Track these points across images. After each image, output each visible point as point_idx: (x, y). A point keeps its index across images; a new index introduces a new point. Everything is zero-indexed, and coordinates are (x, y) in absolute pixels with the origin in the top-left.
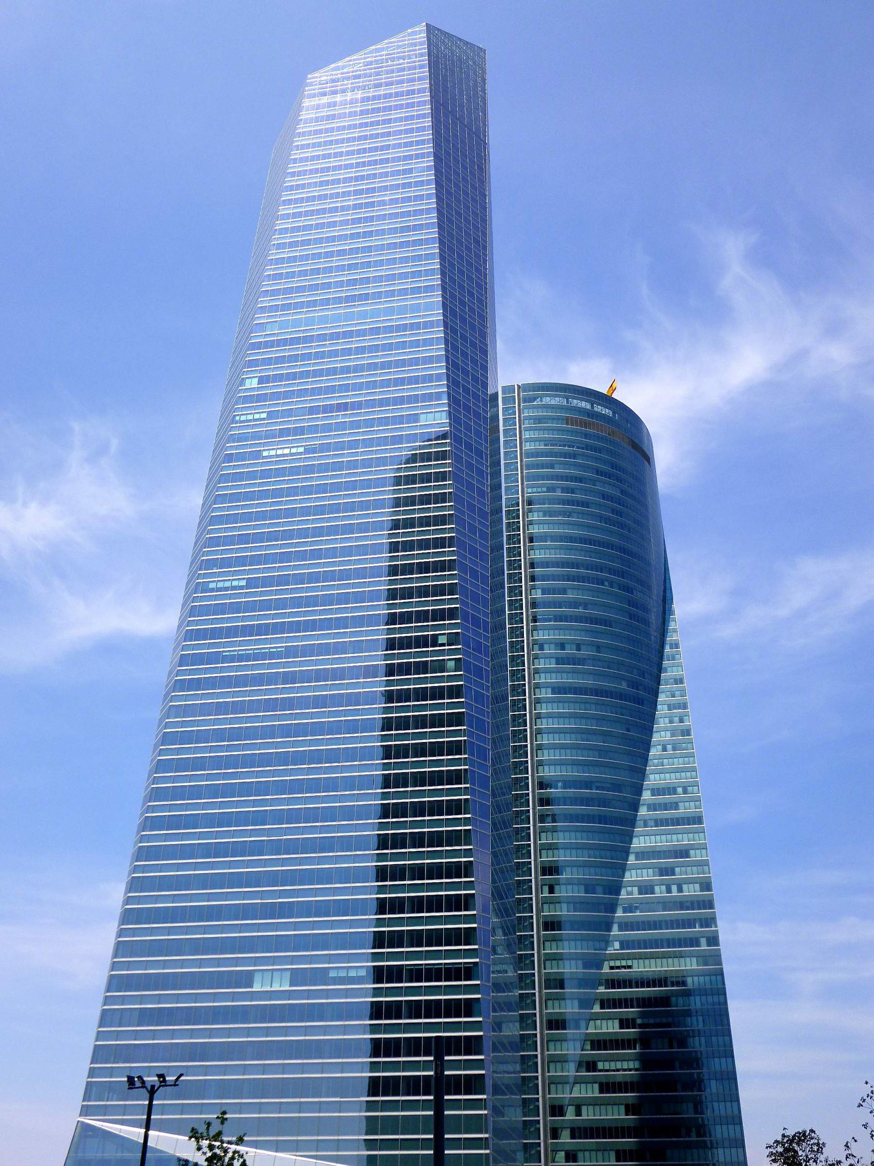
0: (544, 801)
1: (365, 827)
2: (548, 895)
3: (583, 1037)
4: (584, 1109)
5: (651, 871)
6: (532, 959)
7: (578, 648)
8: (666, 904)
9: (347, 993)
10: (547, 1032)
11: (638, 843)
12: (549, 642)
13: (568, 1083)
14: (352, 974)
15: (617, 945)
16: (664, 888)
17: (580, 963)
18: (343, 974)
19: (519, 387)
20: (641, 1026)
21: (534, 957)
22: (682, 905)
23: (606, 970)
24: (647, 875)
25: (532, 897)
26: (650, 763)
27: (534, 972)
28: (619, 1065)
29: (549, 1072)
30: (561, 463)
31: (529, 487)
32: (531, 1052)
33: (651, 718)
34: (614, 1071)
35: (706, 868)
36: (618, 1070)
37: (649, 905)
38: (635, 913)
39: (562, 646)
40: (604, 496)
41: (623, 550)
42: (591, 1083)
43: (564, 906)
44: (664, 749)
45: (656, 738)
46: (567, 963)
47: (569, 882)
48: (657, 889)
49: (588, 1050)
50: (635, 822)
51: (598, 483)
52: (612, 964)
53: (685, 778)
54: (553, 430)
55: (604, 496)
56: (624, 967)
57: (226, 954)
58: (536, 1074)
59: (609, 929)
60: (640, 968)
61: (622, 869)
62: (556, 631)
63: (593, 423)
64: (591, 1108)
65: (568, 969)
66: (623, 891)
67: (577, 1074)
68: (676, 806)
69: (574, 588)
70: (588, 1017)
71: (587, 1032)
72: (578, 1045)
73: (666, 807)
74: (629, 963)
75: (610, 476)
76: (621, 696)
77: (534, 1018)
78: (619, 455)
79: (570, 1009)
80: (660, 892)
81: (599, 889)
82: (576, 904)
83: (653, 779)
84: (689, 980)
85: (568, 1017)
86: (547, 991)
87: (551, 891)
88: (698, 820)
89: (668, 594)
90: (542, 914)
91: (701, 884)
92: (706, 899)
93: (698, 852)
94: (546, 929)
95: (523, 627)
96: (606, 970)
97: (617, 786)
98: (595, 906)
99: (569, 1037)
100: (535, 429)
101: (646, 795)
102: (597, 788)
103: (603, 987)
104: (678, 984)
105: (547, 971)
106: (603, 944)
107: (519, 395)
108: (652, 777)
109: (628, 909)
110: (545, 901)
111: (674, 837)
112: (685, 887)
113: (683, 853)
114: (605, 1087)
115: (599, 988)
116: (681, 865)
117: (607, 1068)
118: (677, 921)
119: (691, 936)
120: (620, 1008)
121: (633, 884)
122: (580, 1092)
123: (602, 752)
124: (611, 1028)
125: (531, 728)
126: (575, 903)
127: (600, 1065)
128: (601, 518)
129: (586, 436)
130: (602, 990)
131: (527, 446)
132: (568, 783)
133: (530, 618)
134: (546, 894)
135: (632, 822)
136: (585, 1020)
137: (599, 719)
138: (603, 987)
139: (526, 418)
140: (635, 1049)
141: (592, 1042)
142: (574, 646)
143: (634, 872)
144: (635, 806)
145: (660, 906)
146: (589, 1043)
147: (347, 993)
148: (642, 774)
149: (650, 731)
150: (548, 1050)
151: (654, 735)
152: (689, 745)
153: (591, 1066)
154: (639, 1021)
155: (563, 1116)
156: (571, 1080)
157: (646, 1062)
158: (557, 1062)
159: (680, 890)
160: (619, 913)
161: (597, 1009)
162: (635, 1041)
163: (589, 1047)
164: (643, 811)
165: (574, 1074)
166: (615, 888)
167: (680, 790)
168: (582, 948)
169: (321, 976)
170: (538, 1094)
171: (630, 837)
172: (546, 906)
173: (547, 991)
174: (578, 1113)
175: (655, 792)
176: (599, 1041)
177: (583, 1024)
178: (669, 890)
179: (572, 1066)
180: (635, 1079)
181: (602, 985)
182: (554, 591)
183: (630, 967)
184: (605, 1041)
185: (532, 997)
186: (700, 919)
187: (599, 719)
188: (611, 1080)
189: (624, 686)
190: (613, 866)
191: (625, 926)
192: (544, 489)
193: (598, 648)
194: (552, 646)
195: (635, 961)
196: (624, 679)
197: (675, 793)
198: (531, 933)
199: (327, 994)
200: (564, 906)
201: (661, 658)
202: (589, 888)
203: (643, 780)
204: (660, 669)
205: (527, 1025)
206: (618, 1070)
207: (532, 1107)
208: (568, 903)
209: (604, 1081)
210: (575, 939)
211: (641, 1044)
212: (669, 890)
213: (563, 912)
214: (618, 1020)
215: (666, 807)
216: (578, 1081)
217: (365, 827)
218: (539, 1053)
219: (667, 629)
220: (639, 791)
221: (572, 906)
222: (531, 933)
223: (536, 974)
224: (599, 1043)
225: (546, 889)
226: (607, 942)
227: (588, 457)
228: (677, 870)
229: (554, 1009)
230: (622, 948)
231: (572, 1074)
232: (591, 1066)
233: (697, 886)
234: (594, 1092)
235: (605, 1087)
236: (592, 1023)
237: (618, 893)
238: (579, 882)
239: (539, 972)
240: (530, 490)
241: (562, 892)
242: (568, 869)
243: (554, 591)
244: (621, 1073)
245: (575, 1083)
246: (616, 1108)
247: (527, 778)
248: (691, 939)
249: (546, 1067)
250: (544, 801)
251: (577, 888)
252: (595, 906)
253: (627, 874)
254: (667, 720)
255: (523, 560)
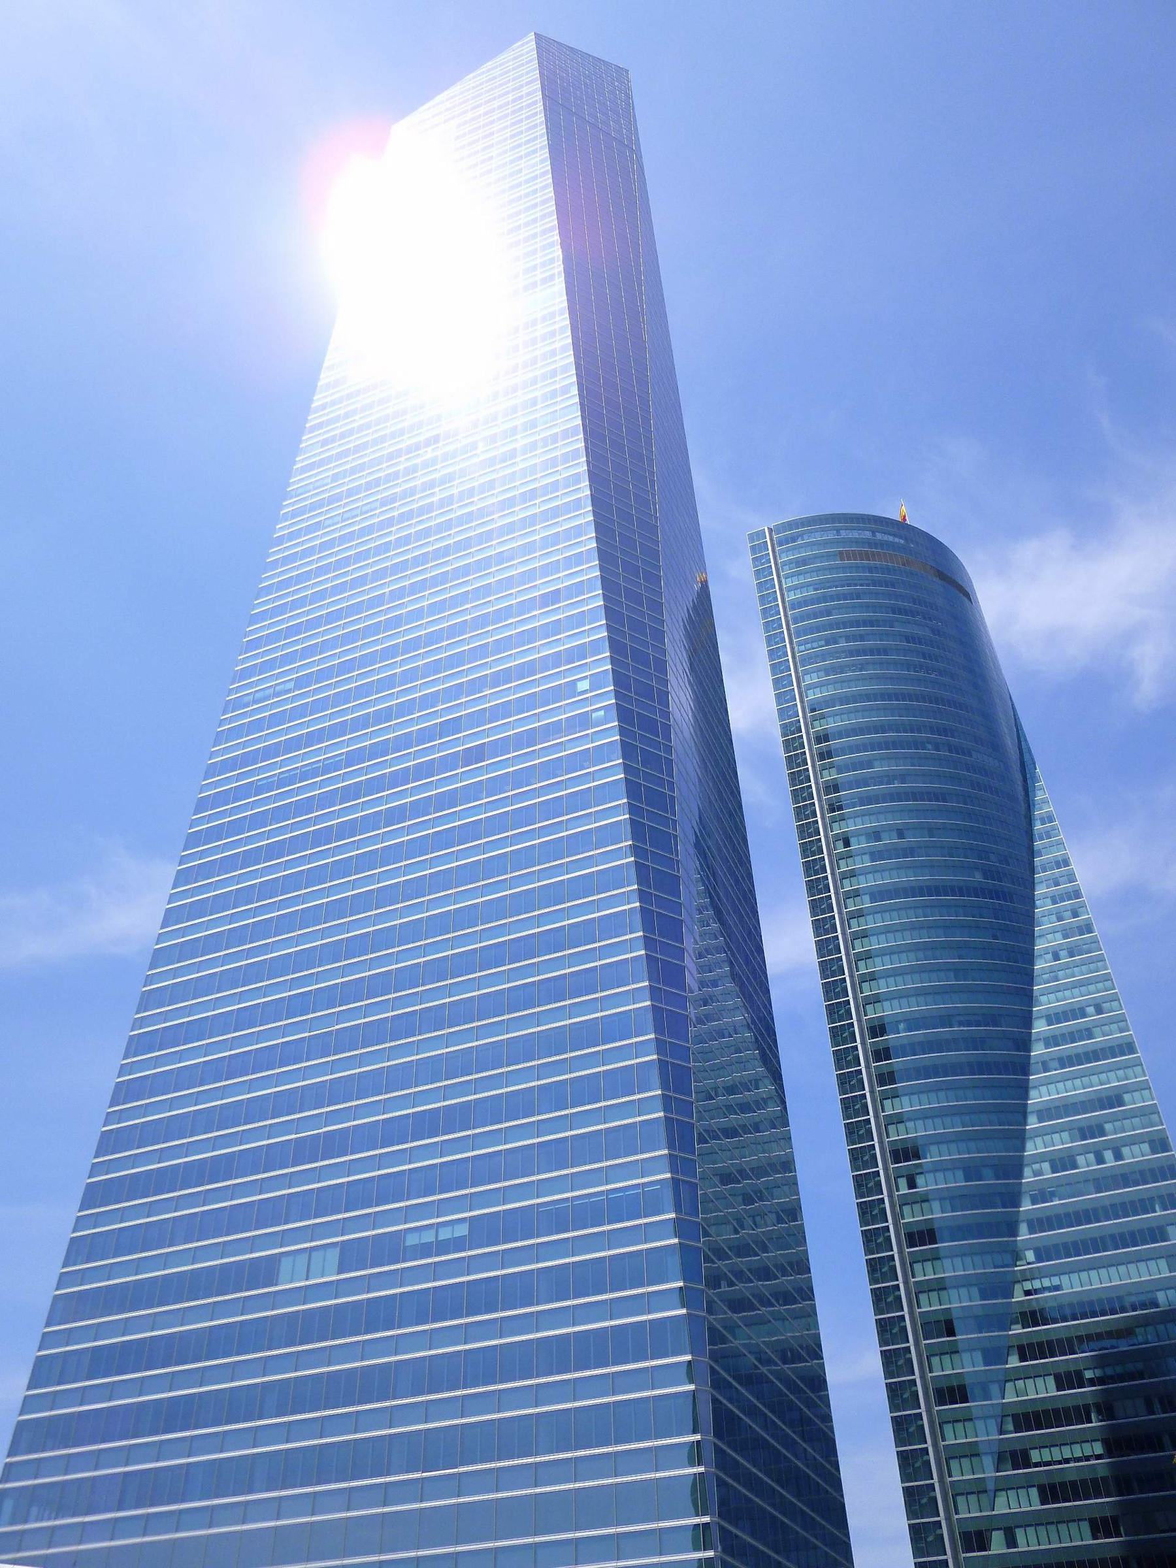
0: (882, 1054)
1: (657, 1458)
2: (907, 1192)
3: (998, 1411)
4: (1020, 1534)
5: (1065, 1135)
6: (920, 1423)
7: (901, 835)
8: (1099, 1182)
9: (436, 1271)
10: (908, 1250)
11: (1038, 1098)
12: (857, 833)
13: (986, 1491)
14: (445, 1234)
15: (1030, 1255)
16: (1091, 1157)
17: (975, 1291)
18: (428, 1237)
19: (770, 530)
20: (1092, 1382)
21: (874, 1149)
22: (1124, 1179)
23: (1019, 1297)
24: (1061, 1143)
25: (874, 1145)
26: (1036, 980)
27: (873, 1143)
28: (1067, 1452)
29: (898, 1190)
30: (840, 607)
31: (800, 644)
32: (894, 1312)
33: (1030, 919)
34: (1060, 1463)
35: (1155, 1117)
36: (1067, 1461)
37: (1073, 1186)
38: (1052, 1201)
39: (876, 835)
40: (908, 638)
41: (997, 894)
42: (1024, 1487)
43: (936, 1205)
44: (1056, 957)
45: (1040, 946)
46: (953, 1293)
47: (938, 1168)
48: (1080, 1160)
49: (1011, 1432)
50: (1029, 1066)
51: (896, 624)
52: (1028, 1286)
53: (1096, 994)
54: (824, 569)
55: (908, 638)
56: (1049, 1289)
57: (445, 1319)
58: (913, 1377)
59: (1014, 1232)
60: (1073, 1286)
61: (1020, 1138)
62: (898, 978)
63: (879, 554)
64: (1031, 1530)
65: (958, 1302)
66: (1027, 1171)
67: (998, 1474)
68: (1088, 1033)
69: (882, 758)
70: (1001, 1377)
71: (1004, 1401)
72: (993, 1425)
73: (1072, 1037)
74: (1056, 1281)
75: (912, 613)
76: (977, 891)
77: (938, 1532)
78: (922, 577)
79: (969, 1366)
80: (1086, 1165)
81: (987, 1172)
82: (954, 1199)
83: (1045, 1003)
84: (1161, 1297)
85: (968, 1381)
86: (928, 1342)
87: (912, 1184)
88: (1129, 1048)
89: (1026, 757)
90: (902, 1221)
91: (1152, 1143)
92: (1155, 1138)
93: (1137, 1095)
94: (941, 1402)
95: (817, 822)
96: (1019, 1297)
97: (993, 1019)
98: (983, 1199)
99: (975, 1413)
100: (799, 574)
101: (1040, 1027)
102: (960, 1024)
103: (1020, 1326)
104: (1143, 1306)
105: (891, 1139)
106: (1008, 1258)
107: (771, 539)
108: (1043, 999)
109: (1041, 1196)
110: (905, 1201)
111: (1094, 1079)
112: (1125, 1151)
113: (1114, 1099)
114: (1050, 1492)
115: (1013, 1327)
116: (1113, 1119)
117: (1047, 1458)
118: (1123, 1204)
119: (1154, 1224)
120: (1052, 1357)
121: (1040, 1158)
122: (1005, 1505)
123: (959, 972)
124: (1043, 1390)
125: (840, 913)
126: (952, 1198)
127: (1035, 1456)
128: (908, 666)
129: (870, 570)
130: (1017, 1330)
131: (791, 597)
132: (913, 1023)
133: (826, 807)
134: (904, 1190)
135: (1024, 1068)
136: (998, 1381)
137: (947, 927)
138: (1020, 1326)
139: (784, 564)
140: (1118, 1535)
141: (1015, 1417)
142: (895, 834)
143: (1039, 1141)
144: (1024, 1044)
145: (1091, 1187)
146: (1010, 1419)
147: (436, 1271)
148: (1028, 997)
149: (1031, 938)
150: (919, 1307)
151: (1037, 941)
152: (1115, 1004)
153: (1020, 1458)
154: (1088, 1374)
155: (985, 1550)
156: (991, 1486)
157: (1114, 1444)
158: (914, 1203)
159: (1118, 1156)
160: (1026, 1206)
161: (1014, 1362)
162: (1115, 1520)
163: (1011, 1427)
164: (1038, 1051)
165: (993, 1474)
166: (1014, 1168)
167: (1091, 1010)
168: (913, 982)
169: (390, 1248)
170: (908, 1341)
171: (1024, 1090)
172: (906, 1209)
173: (928, 1342)
174: (1011, 1542)
175: (1051, 1019)
176: (1026, 1415)
177: (995, 1389)
178: (1100, 1160)
179: (988, 1462)
180: (1117, 1553)
181: (1017, 1323)
182: (855, 765)
183: (1057, 1288)
184: (1036, 1414)
185: (849, 1029)
186: (1161, 1197)
187: (947, 927)
188: (1057, 1480)
189: (978, 877)
190: (1006, 1136)
191: (1038, 1224)
192: (823, 643)
193: (931, 831)
194: (863, 838)
195: (1065, 1278)
196: (977, 869)
197: (1084, 1015)
198: (858, 1068)
199: (402, 1277)
200: (936, 1205)
201: (1031, 839)
202: (971, 1171)
203: (1031, 1006)
204: (1032, 853)
205: (904, 1401)
206: (1067, 1461)
207: (930, 1539)
208: (941, 1199)
209: (1044, 1481)
210: (962, 1254)
211: (1099, 1412)
212: (1100, 1160)
213: (936, 1213)
214: (1052, 1377)
215: (1072, 1037)
216: (1004, 1486)
217: (657, 1458)
218: (929, 1444)
219: (1033, 800)
220: (1027, 1020)
221: (947, 1204)
222: (858, 1068)
223: (913, 1349)
224: (1029, 1418)
225: (903, 1182)
226: (1017, 1256)
227: (876, 594)
228: (1108, 1127)
229: (944, 1369)
230: (1039, 1259)
231: (989, 1475)
232: (1020, 1458)
233: (1146, 1147)
234: (1030, 1502)
235: (1050, 1492)
236: (1009, 1385)
237: (1020, 1175)
238: (952, 1166)
239: (923, 1377)
240: (802, 648)
241: (924, 1184)
242: (934, 1149)
243: (855, 765)
244: (1072, 1465)
245: (996, 1491)
246: (1073, 1526)
247: (864, 1096)
248: (1151, 1230)
249: (884, 1130)
250: (882, 1054)
251: (941, 1122)
252: (983, 1199)
253: (1029, 1145)
254: (1054, 918)
255: (813, 786)
